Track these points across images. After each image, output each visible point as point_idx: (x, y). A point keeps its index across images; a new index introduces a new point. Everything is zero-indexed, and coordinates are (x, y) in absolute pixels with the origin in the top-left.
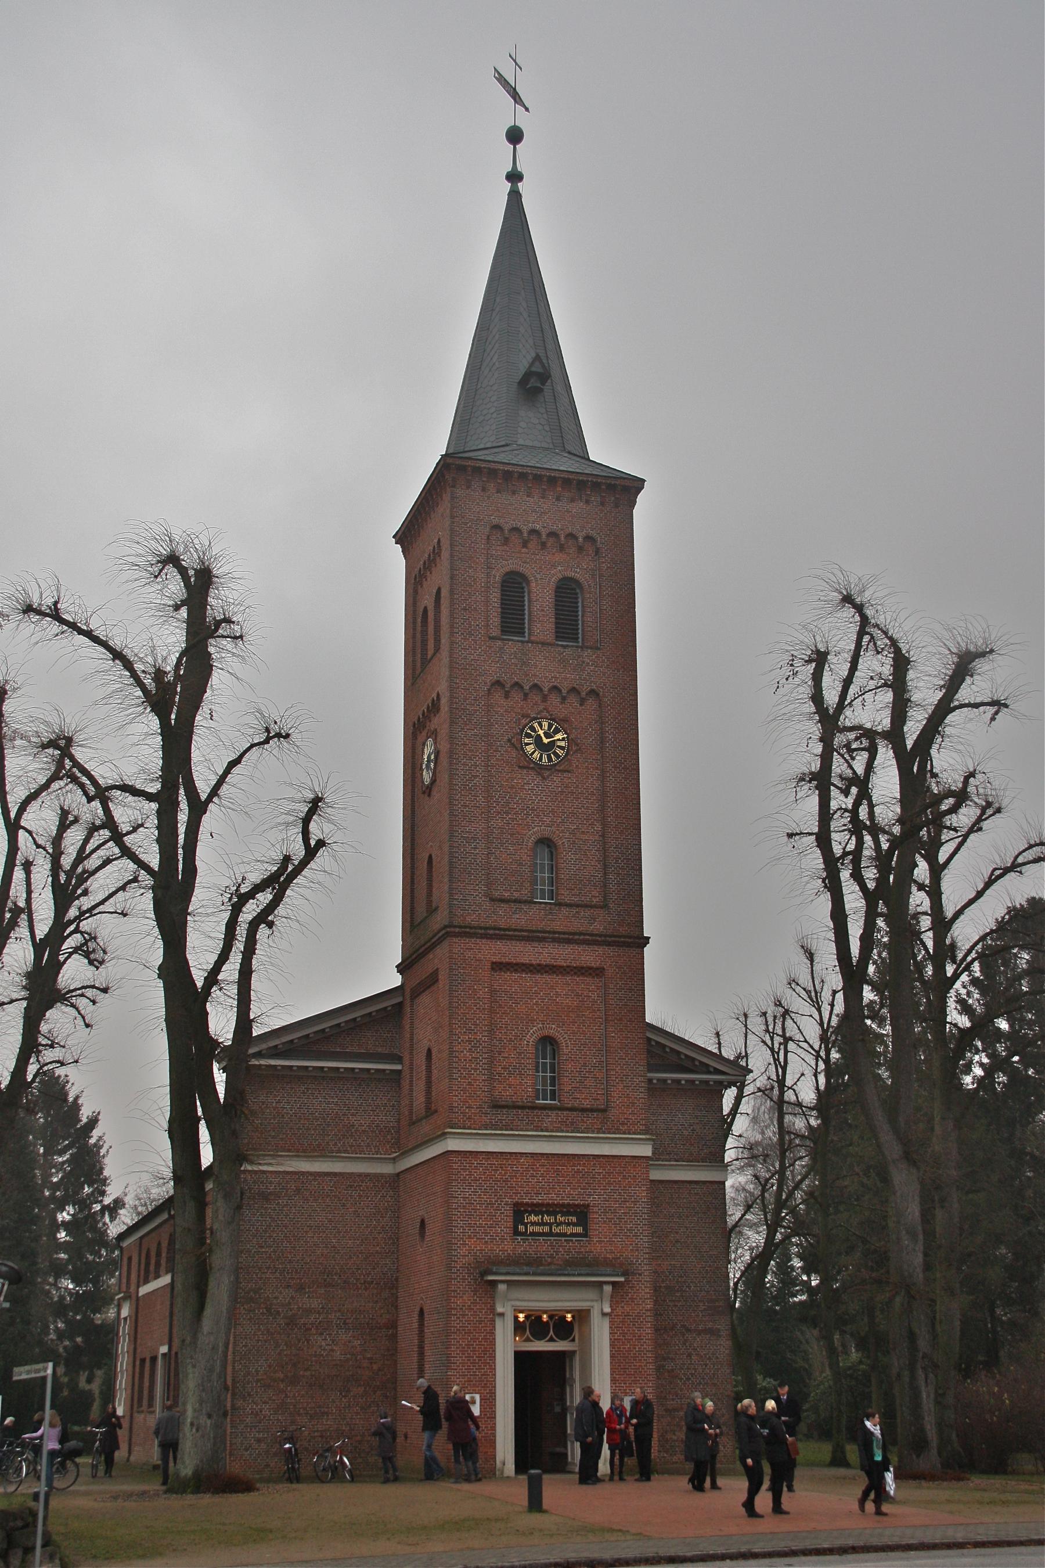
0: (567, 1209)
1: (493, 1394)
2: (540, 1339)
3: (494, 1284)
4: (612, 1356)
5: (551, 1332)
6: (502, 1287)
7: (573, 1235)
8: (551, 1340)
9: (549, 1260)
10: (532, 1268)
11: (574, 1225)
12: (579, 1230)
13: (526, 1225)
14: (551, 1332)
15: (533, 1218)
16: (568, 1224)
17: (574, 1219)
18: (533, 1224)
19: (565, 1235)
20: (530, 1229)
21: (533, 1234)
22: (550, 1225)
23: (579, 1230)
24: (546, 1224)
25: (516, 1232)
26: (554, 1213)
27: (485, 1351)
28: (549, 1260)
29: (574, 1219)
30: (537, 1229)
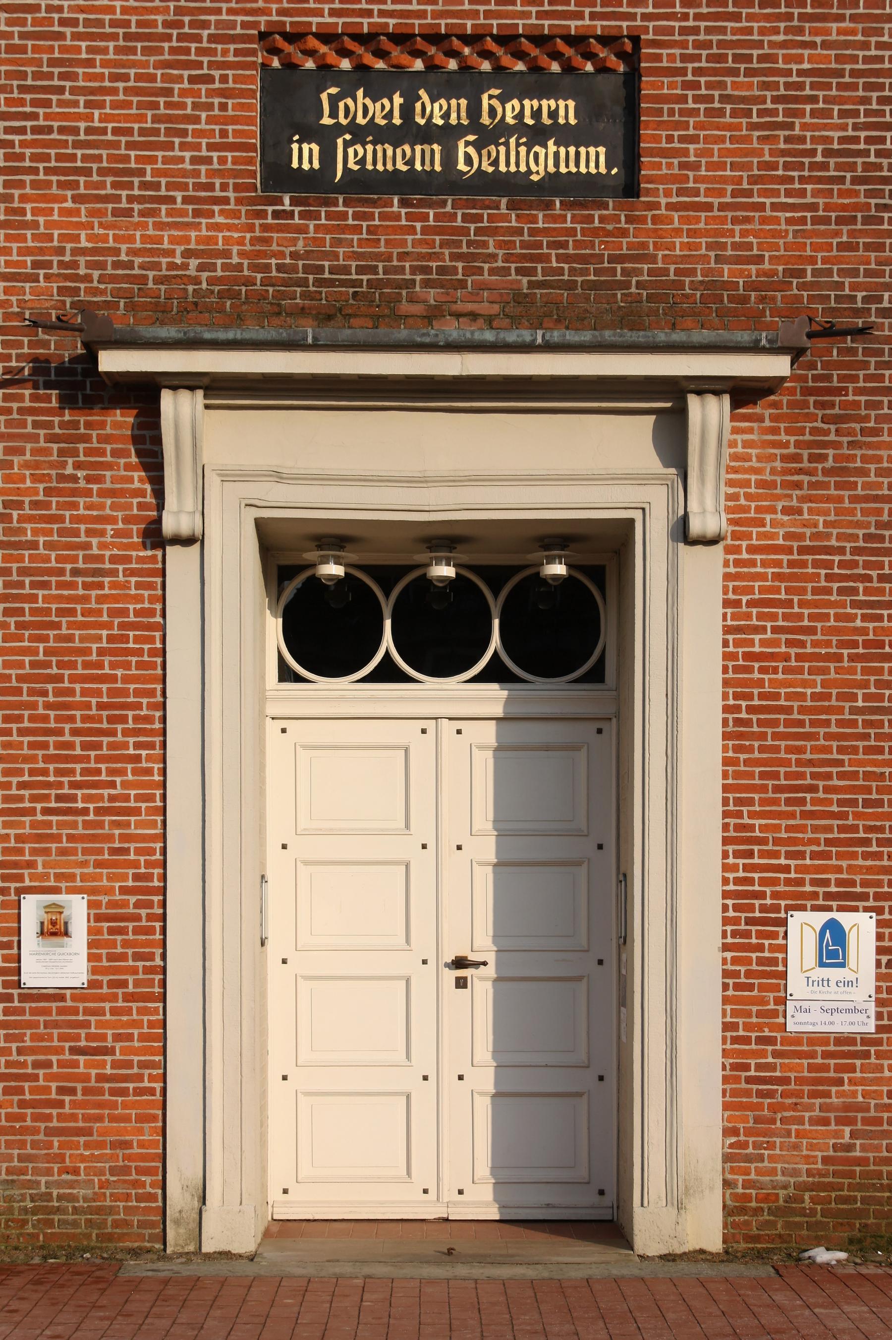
0: (535, 59)
1: (154, 891)
2: (290, 634)
3: (143, 393)
4: (736, 733)
5: (388, 641)
6: (176, 407)
7: (556, 184)
8: (387, 673)
9: (432, 295)
10: (334, 326)
11: (566, 136)
12: (594, 160)
13: (326, 139)
14: (388, 641)
15: (363, 107)
16: (537, 134)
17: (567, 110)
18: (359, 134)
19: (515, 188)
20: (350, 157)
21: (365, 185)
22: (447, 135)
23: (594, 160)
24: (427, 134)
25: (279, 176)
26: (467, 84)
27: (116, 709)
28: (432, 295)
29: (567, 110)
30: (392, 158)
